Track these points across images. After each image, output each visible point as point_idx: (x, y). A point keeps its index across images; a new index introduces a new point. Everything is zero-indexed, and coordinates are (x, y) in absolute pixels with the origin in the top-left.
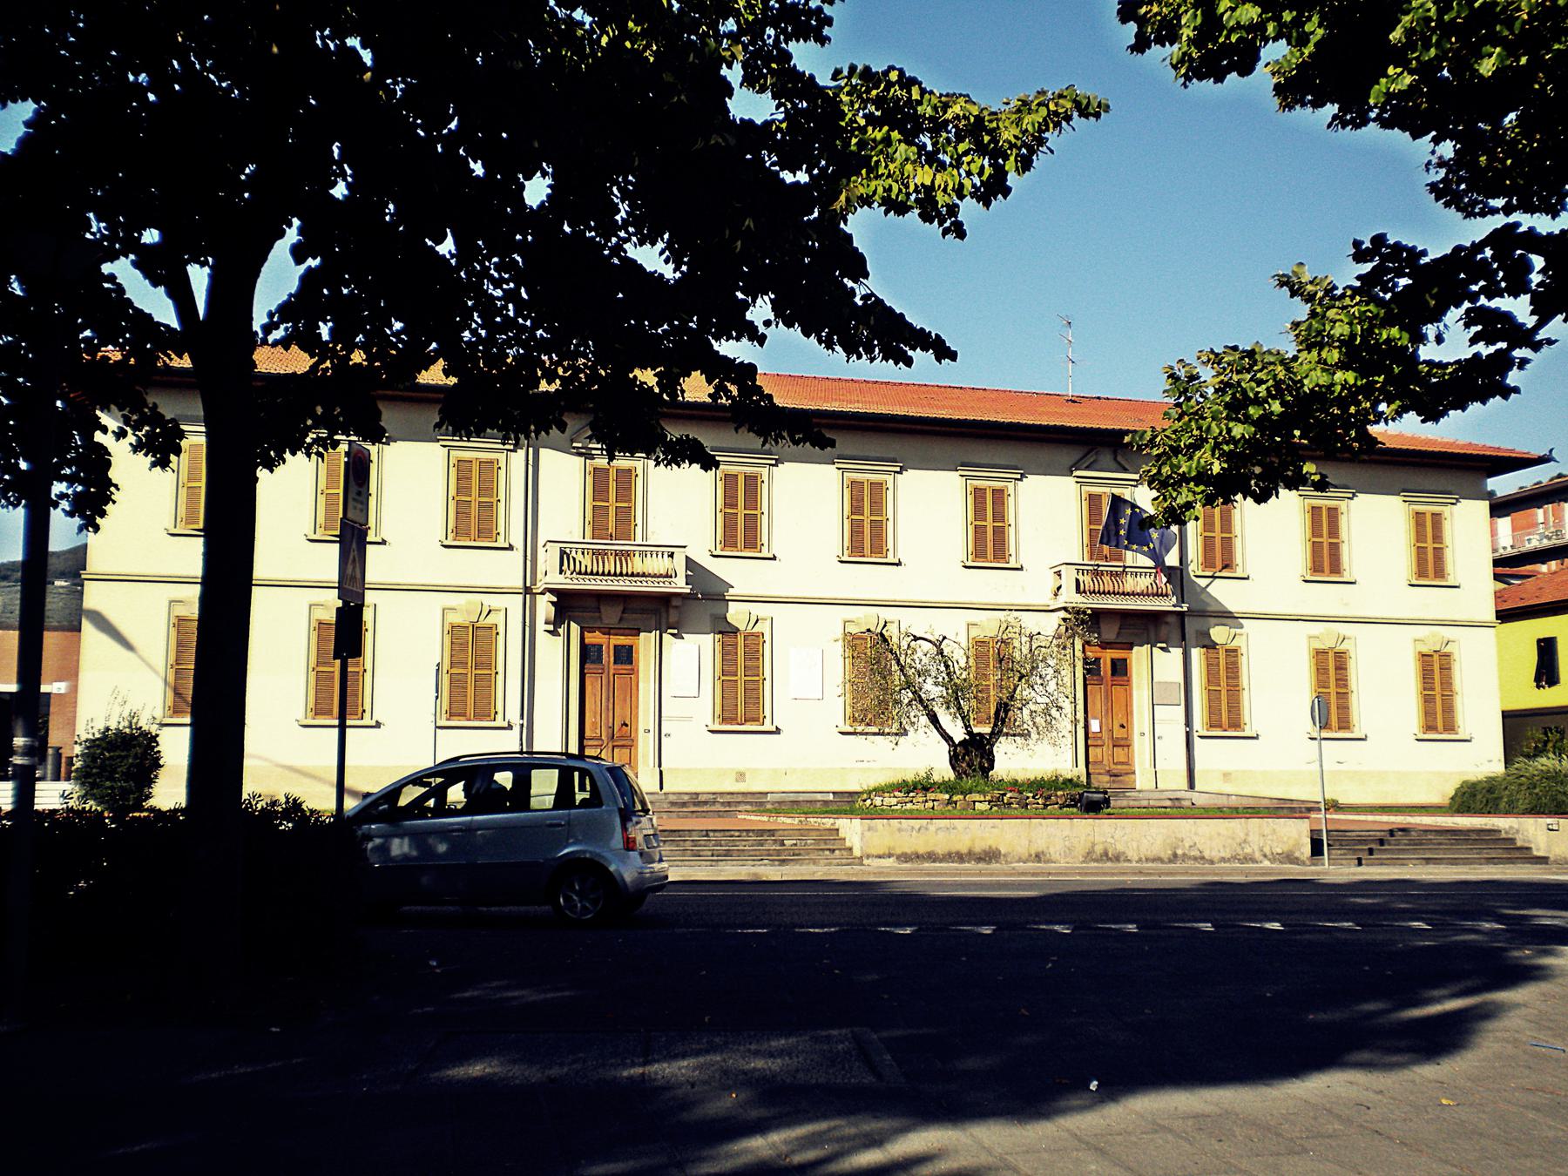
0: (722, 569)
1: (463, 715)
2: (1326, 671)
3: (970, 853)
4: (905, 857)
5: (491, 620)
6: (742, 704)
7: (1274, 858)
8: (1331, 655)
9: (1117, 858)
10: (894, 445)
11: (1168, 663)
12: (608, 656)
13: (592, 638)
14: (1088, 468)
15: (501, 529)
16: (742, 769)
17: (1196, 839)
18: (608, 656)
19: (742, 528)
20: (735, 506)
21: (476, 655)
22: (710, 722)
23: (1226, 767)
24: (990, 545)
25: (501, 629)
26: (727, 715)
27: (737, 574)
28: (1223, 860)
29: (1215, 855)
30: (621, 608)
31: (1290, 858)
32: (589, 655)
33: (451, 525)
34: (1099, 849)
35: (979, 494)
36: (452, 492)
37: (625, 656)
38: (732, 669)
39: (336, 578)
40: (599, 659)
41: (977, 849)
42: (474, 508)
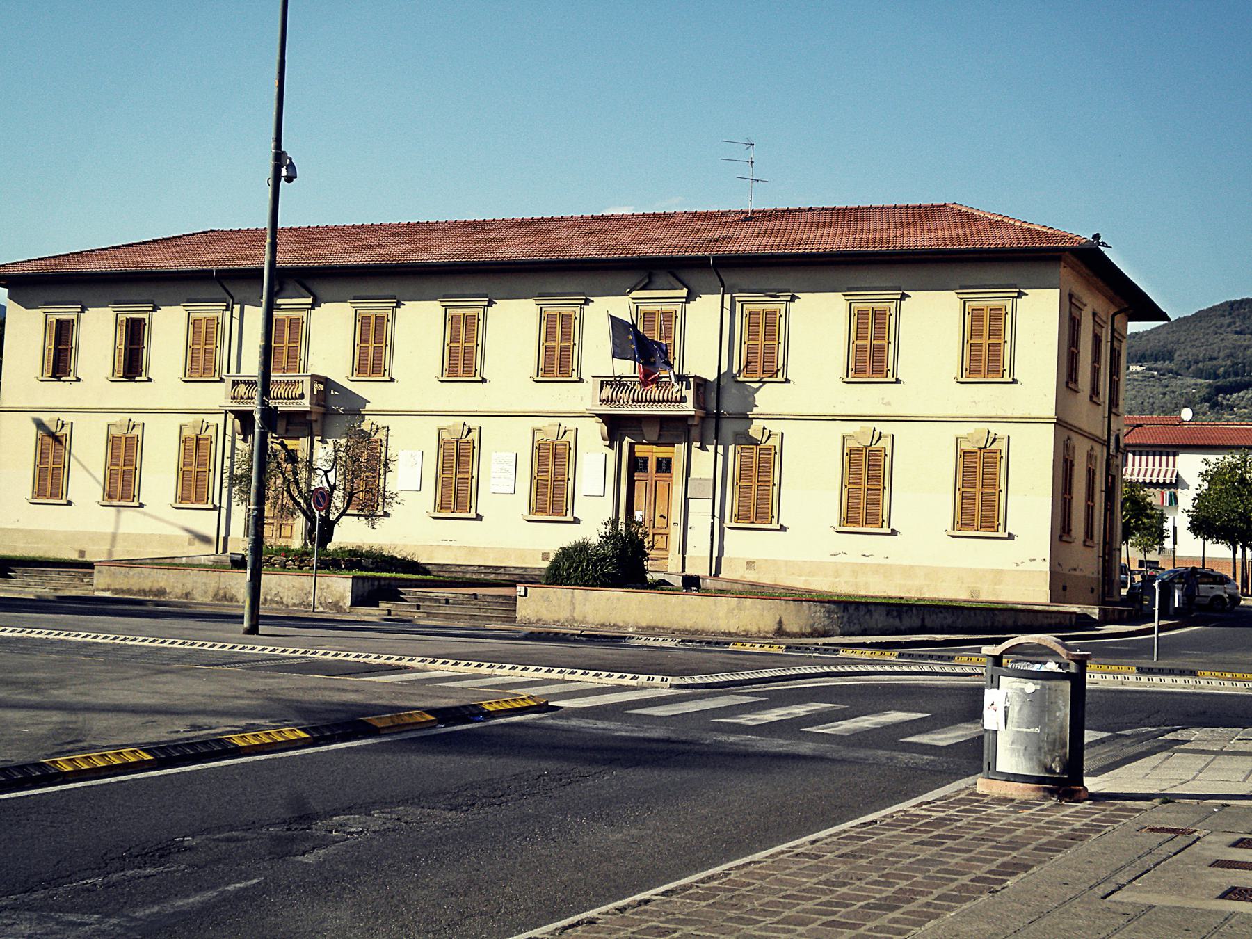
0: (358, 389)
1: (543, 511)
2: (859, 468)
3: (150, 590)
4: (115, 591)
5: (880, 445)
6: (756, 505)
7: (327, 605)
8: (123, 440)
9: (231, 599)
10: (484, 284)
11: (703, 462)
12: (652, 465)
13: (640, 451)
14: (643, 288)
15: (1007, 367)
16: (751, 557)
17: (280, 589)
18: (652, 465)
19: (372, 355)
20: (367, 341)
21: (197, 457)
22: (526, 513)
23: (748, 551)
24: (557, 362)
25: (1004, 454)
26: (965, 521)
27: (373, 394)
28: (294, 605)
29: (291, 602)
30: (658, 428)
31: (336, 606)
32: (637, 465)
33: (446, 366)
34: (221, 593)
35: (551, 319)
36: (358, 341)
37: (664, 465)
38: (766, 478)
39: (1052, 414)
40: (645, 469)
41: (154, 589)
42: (371, 351)
